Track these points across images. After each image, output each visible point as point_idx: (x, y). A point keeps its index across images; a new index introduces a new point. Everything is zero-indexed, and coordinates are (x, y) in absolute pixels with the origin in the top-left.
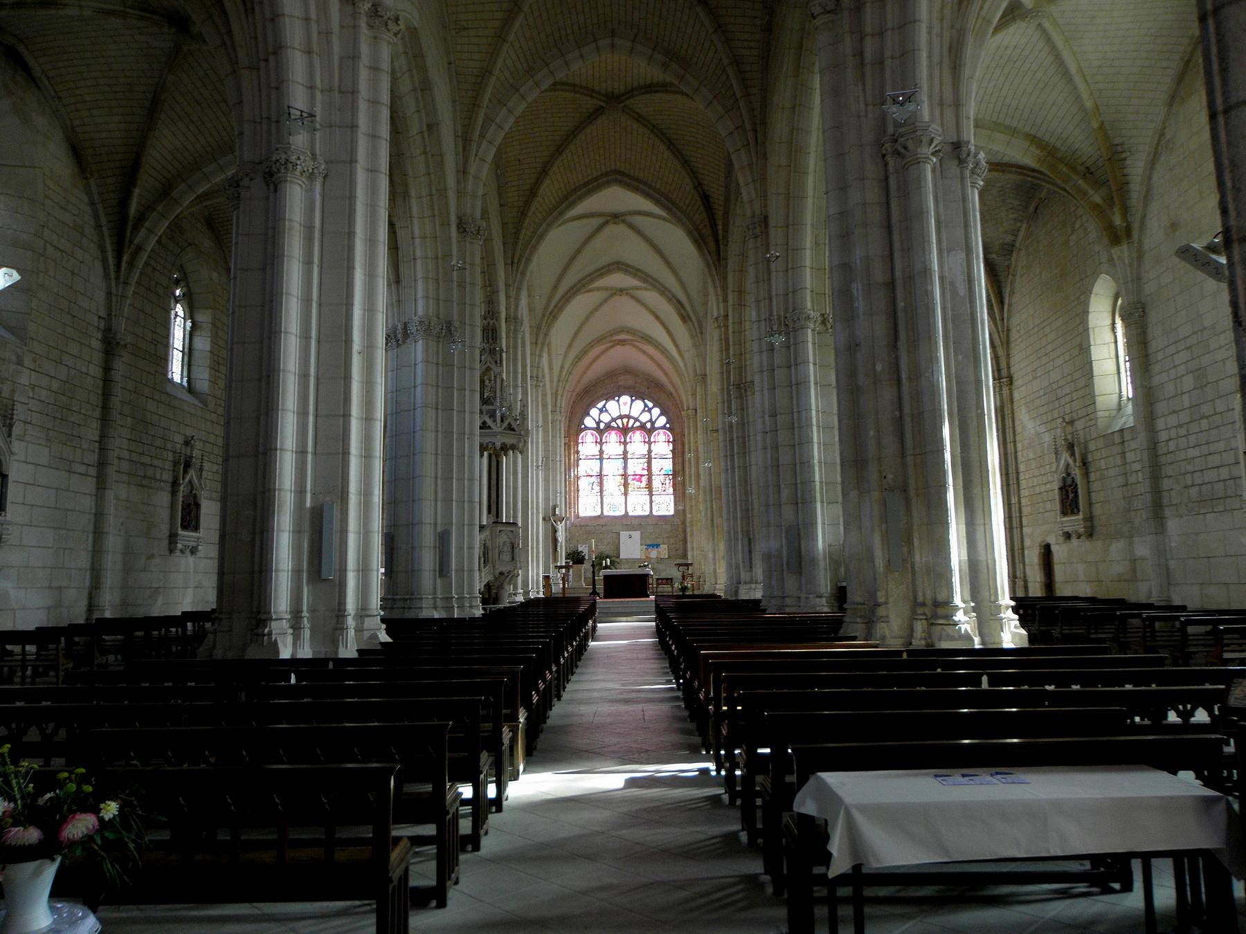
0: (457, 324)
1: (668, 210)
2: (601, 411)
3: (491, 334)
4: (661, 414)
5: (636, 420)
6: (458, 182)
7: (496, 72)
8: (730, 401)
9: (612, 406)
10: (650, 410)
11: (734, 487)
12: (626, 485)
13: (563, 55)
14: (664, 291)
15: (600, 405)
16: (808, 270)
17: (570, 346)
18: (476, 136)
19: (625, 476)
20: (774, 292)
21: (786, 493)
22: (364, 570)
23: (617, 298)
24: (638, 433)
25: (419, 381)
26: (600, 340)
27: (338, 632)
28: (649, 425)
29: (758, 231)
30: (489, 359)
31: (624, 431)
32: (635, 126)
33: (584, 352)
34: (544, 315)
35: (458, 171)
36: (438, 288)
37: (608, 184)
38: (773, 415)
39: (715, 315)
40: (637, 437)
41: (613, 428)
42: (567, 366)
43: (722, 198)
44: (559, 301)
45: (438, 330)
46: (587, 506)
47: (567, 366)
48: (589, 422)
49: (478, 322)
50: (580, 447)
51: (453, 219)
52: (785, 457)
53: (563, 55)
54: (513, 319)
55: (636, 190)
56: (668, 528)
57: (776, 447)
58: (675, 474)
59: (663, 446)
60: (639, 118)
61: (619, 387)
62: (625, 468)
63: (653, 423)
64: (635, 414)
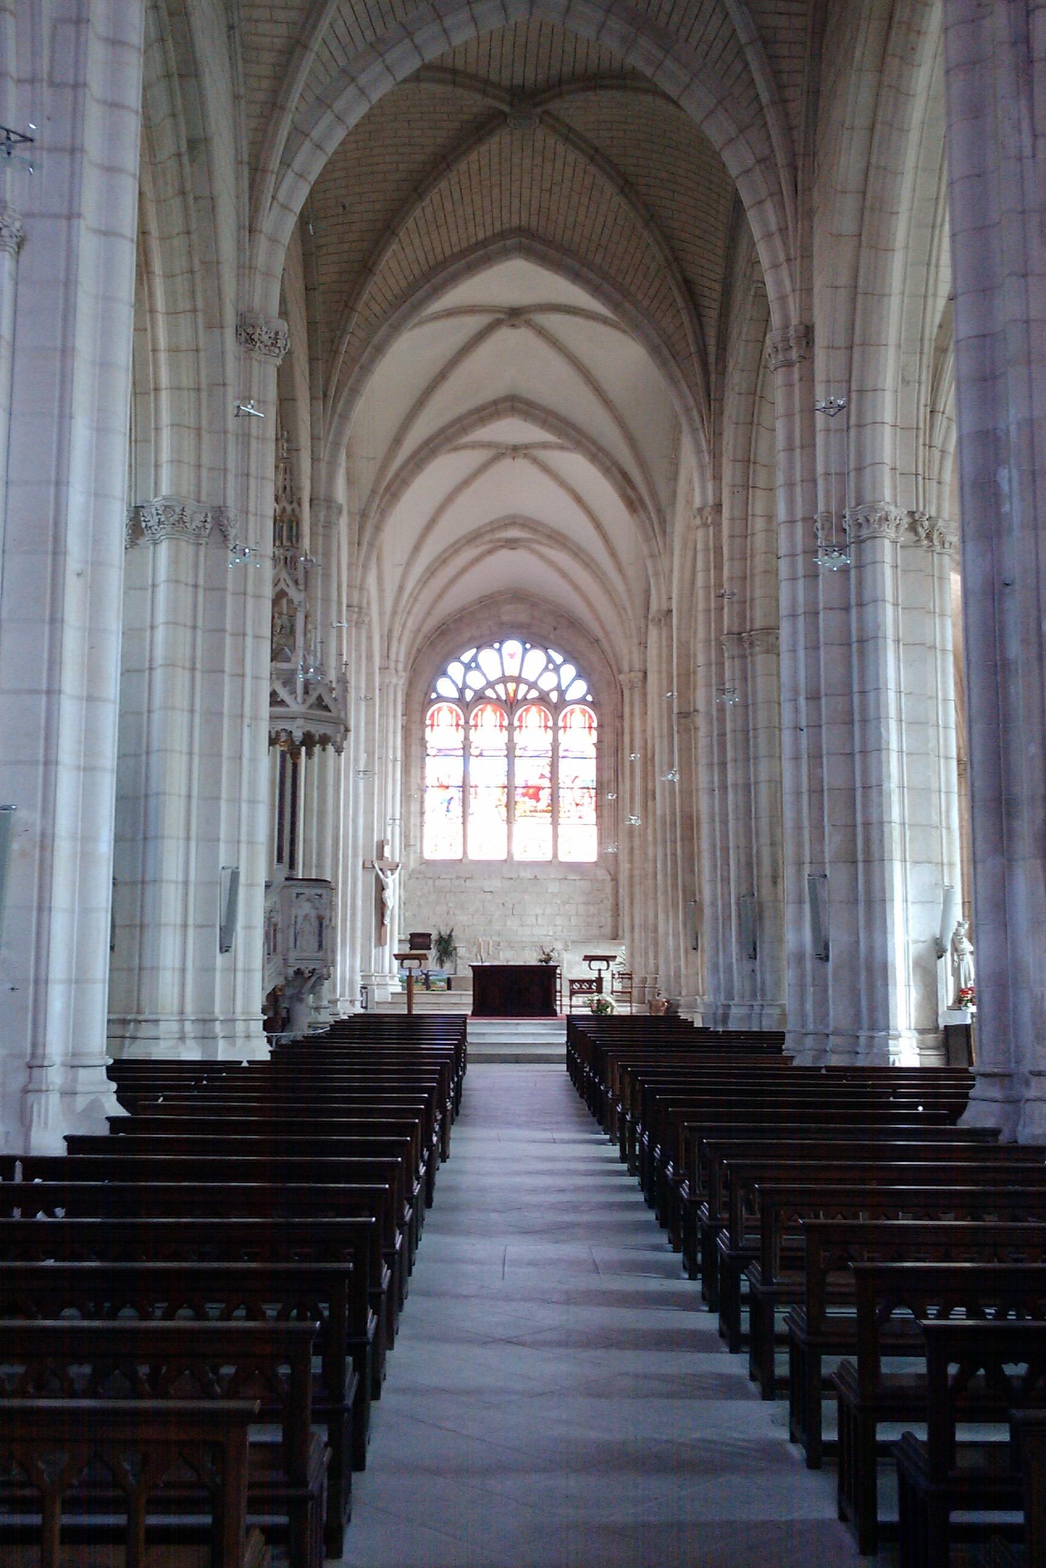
0: (232, 513)
1: (616, 306)
2: (468, 667)
3: (287, 528)
4: (579, 676)
5: (532, 685)
6: (240, 248)
7: (316, 45)
8: (721, 664)
9: (488, 657)
10: (557, 669)
11: (725, 822)
12: (510, 805)
13: (439, 17)
14: (597, 453)
15: (466, 657)
16: (887, 429)
17: (417, 548)
18: (274, 164)
19: (509, 788)
20: (820, 469)
21: (833, 843)
22: (79, 981)
23: (507, 463)
24: (534, 709)
25: (161, 617)
26: (472, 538)
27: (31, 1097)
28: (554, 697)
29: (794, 354)
30: (284, 575)
31: (510, 705)
32: (561, 148)
33: (443, 560)
34: (373, 492)
35: (240, 228)
36: (199, 448)
37: (505, 253)
38: (814, 697)
39: (697, 502)
40: (533, 717)
41: (489, 701)
42: (410, 585)
43: (718, 287)
44: (403, 467)
45: (197, 523)
46: (440, 841)
47: (410, 585)
48: (445, 687)
49: (269, 507)
50: (429, 734)
51: (230, 319)
52: (831, 775)
53: (439, 17)
54: (323, 501)
55: (556, 266)
56: (585, 885)
57: (816, 757)
58: (601, 788)
59: (580, 737)
60: (569, 135)
61: (501, 625)
62: (510, 773)
63: (562, 693)
64: (529, 675)
